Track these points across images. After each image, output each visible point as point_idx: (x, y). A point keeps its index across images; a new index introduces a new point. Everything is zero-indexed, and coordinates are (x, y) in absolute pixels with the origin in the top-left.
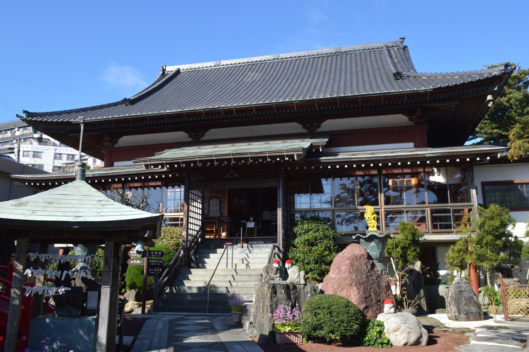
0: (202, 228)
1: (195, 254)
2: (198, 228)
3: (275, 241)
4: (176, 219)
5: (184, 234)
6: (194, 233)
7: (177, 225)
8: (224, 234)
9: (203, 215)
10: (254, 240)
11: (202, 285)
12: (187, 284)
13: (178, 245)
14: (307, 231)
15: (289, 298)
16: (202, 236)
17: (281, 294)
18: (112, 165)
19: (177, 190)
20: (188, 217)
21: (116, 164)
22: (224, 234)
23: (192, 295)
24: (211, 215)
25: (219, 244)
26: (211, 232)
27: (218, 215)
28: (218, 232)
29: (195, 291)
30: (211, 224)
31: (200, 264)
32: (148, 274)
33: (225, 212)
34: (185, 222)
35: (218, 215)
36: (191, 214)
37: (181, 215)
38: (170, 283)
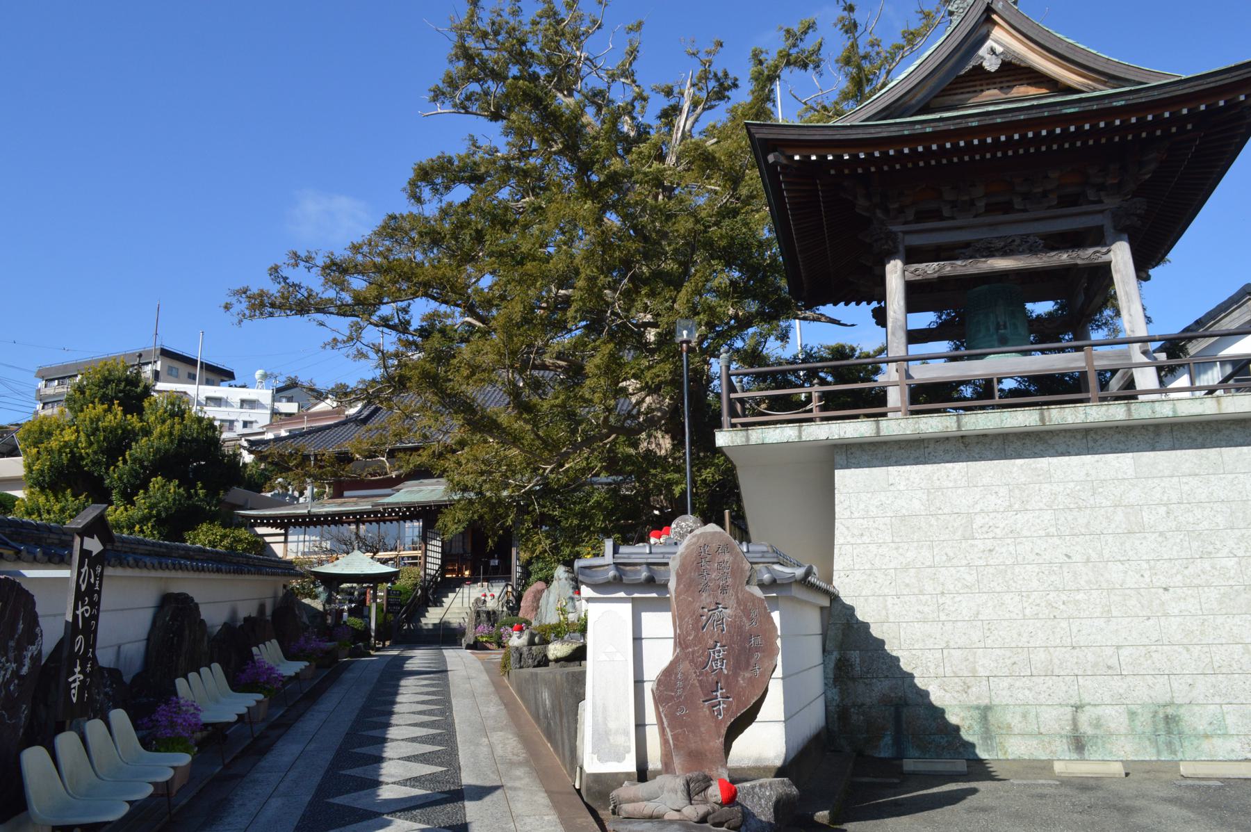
0: (442, 567)
1: (433, 594)
2: (94, 727)
3: (509, 579)
4: (415, 558)
5: (422, 573)
6: (433, 572)
7: (415, 564)
8: (467, 573)
9: (443, 553)
10: (495, 579)
11: (437, 621)
12: (424, 621)
13: (416, 585)
14: (541, 570)
15: (489, 620)
16: (442, 575)
17: (483, 617)
18: (341, 496)
19: (416, 524)
20: (426, 556)
21: (346, 493)
22: (467, 573)
23: (428, 630)
24: (453, 552)
25: (459, 583)
26: (452, 571)
27: (461, 551)
28: (460, 571)
29: (430, 627)
30: (453, 563)
31: (438, 603)
32: (388, 611)
33: (469, 549)
34: (422, 561)
35: (461, 551)
36: (429, 553)
37: (418, 553)
38: (408, 620)
